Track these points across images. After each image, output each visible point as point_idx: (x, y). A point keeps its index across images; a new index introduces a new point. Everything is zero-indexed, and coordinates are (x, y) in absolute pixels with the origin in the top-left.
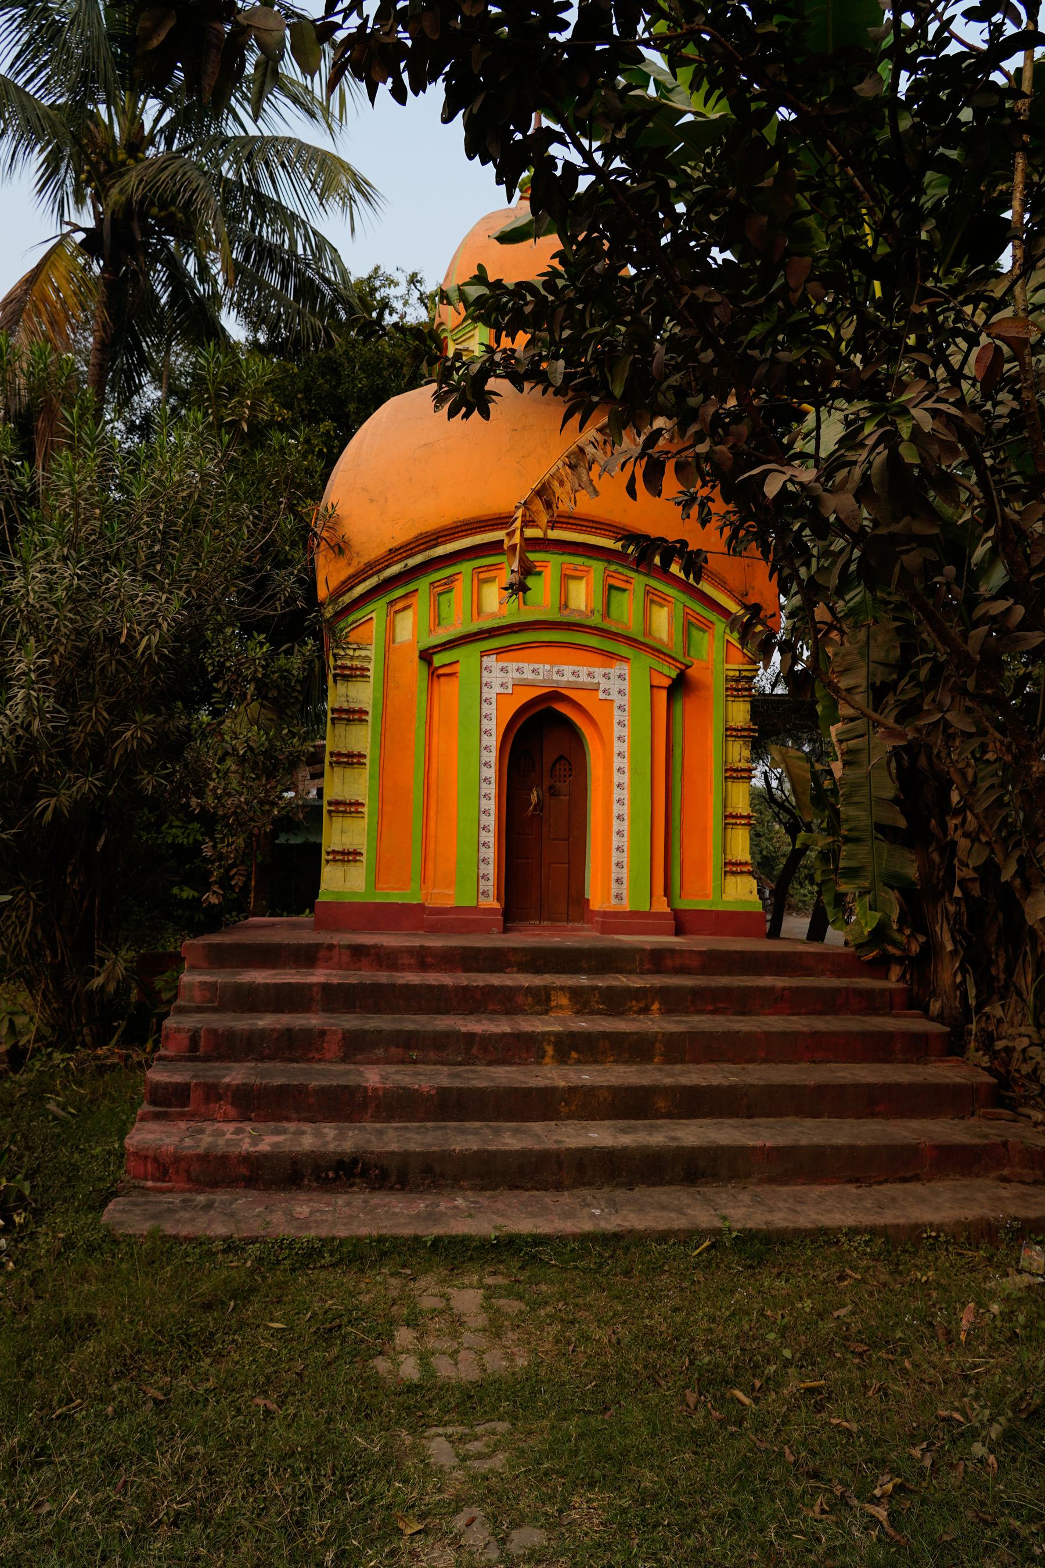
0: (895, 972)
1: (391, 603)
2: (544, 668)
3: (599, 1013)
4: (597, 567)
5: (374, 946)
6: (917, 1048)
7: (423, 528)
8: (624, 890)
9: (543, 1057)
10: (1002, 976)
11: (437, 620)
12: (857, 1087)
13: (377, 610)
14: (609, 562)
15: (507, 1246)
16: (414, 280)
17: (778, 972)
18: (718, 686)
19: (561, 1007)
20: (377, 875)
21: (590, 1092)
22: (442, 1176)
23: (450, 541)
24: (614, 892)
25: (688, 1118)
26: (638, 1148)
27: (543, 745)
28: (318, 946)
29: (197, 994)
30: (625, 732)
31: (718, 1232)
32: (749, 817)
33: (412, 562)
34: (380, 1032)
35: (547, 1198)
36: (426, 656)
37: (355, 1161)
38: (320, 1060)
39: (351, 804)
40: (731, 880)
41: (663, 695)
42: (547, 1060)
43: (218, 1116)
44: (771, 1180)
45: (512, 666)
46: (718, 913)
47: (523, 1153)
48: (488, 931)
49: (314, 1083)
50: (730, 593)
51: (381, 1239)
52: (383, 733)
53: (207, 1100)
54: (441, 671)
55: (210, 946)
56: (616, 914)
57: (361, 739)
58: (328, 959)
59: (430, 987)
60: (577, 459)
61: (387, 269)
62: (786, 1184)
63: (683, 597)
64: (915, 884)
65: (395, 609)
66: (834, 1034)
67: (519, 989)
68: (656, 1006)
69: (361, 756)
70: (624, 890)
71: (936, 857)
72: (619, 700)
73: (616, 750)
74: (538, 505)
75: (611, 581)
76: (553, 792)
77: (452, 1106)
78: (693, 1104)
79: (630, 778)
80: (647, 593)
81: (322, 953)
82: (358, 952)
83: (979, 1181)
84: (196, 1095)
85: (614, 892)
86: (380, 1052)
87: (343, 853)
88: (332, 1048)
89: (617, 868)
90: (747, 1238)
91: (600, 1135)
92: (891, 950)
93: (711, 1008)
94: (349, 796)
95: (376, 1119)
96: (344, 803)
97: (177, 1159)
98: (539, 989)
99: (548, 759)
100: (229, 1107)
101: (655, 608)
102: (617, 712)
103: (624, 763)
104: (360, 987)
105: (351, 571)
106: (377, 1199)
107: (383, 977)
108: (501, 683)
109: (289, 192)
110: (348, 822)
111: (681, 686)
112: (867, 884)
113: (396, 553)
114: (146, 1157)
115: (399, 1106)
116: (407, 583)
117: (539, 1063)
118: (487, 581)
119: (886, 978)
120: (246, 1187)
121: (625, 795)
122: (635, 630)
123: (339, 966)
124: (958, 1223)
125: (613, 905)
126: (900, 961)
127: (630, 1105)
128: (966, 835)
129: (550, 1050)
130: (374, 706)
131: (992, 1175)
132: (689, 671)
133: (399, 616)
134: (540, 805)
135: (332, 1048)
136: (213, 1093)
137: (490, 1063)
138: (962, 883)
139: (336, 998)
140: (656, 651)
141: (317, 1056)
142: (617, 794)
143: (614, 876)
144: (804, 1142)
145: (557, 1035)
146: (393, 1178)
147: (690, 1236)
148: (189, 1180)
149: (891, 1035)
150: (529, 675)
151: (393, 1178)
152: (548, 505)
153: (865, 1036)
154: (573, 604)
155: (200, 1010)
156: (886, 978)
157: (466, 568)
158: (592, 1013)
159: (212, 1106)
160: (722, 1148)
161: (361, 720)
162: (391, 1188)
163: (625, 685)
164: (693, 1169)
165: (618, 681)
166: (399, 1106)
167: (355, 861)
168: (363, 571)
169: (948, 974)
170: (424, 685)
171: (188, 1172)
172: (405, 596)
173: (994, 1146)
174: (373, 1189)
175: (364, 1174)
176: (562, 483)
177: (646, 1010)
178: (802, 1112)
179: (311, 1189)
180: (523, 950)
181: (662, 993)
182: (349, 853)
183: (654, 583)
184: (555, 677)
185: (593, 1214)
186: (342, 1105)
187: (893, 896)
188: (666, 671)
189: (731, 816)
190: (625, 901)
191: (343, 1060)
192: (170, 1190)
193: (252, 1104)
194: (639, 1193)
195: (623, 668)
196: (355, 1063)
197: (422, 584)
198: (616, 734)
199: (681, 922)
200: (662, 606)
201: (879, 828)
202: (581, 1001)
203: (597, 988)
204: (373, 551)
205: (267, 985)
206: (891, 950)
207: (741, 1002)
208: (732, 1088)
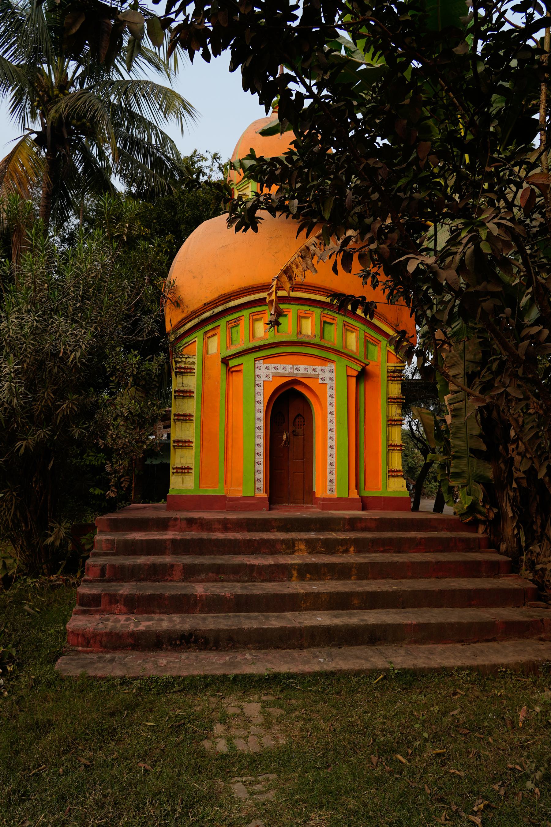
0: (481, 528)
1: (206, 333)
2: (289, 367)
3: (321, 553)
4: (317, 312)
5: (200, 519)
6: (494, 569)
7: (223, 292)
8: (334, 486)
9: (291, 577)
10: (539, 530)
11: (231, 342)
13: (198, 337)
14: (323, 309)
16: (215, 157)
17: (134, 543)
18: (383, 375)
19: (301, 550)
20: (201, 480)
21: (317, 595)
22: (238, 642)
23: (237, 298)
24: (328, 487)
26: (343, 626)
27: (289, 408)
28: (169, 519)
29: (104, 545)
31: (387, 670)
32: (401, 446)
36: (225, 361)
37: (191, 635)
38: (171, 581)
39: (186, 442)
40: (392, 480)
41: (354, 380)
42: (294, 578)
43: (116, 611)
44: (416, 642)
45: (272, 366)
48: (261, 510)
49: (168, 593)
50: (389, 325)
51: (205, 677)
53: (111, 603)
54: (233, 369)
55: (110, 520)
56: (330, 500)
57: (190, 406)
59: (230, 541)
61: (201, 152)
62: (424, 644)
64: (491, 481)
65: (208, 336)
66: (449, 562)
68: (352, 549)
71: (503, 466)
73: (329, 411)
74: (285, 278)
75: (325, 319)
76: (295, 434)
77: (243, 604)
78: (373, 601)
79: (336, 426)
80: (344, 325)
81: (171, 523)
82: (191, 522)
83: (528, 641)
84: (104, 600)
85: (328, 487)
86: (203, 576)
87: (181, 468)
88: (178, 574)
89: (330, 474)
90: (403, 673)
91: (323, 619)
92: (479, 516)
93: (381, 549)
94: (184, 437)
95: (202, 611)
97: (95, 635)
98: (288, 540)
99: (292, 416)
100: (122, 607)
101: (349, 334)
103: (333, 418)
104: (192, 540)
105: (184, 315)
106: (203, 655)
107: (204, 535)
108: (264, 376)
110: (184, 452)
111: (363, 375)
113: (208, 306)
114: (78, 634)
115: (215, 604)
116: (214, 322)
117: (290, 581)
118: (257, 320)
119: (477, 532)
121: (334, 435)
122: (338, 346)
123: (181, 530)
124: (517, 663)
126: (484, 522)
127: (339, 602)
128: (519, 454)
129: (295, 574)
131: (535, 637)
135: (178, 574)
136: (113, 599)
137: (263, 581)
138: (517, 480)
139: (178, 547)
140: (349, 357)
142: (329, 434)
143: (328, 479)
144: (433, 621)
145: (299, 565)
146: (212, 644)
147: (372, 673)
148: (101, 646)
150: (281, 371)
151: (212, 644)
152: (290, 278)
154: (304, 332)
155: (105, 554)
156: (477, 532)
157: (246, 313)
158: (318, 553)
159: (113, 606)
160: (389, 625)
162: (211, 649)
163: (333, 376)
164: (374, 636)
166: (215, 604)
167: (188, 473)
168: (190, 316)
169: (510, 529)
170: (224, 376)
171: (100, 642)
174: (201, 650)
175: (196, 641)
176: (297, 266)
177: (346, 551)
178: (452, 606)
180: (280, 520)
181: (356, 542)
182: (185, 468)
183: (347, 320)
184: (295, 372)
185: (319, 661)
186: (184, 604)
190: (335, 492)
191: (183, 580)
192: (91, 652)
193: (136, 605)
194: (345, 650)
195: (330, 366)
196: (190, 582)
197: (223, 322)
200: (352, 332)
201: (472, 450)
202: (312, 547)
203: (320, 539)
206: (479, 516)
208: (394, 592)
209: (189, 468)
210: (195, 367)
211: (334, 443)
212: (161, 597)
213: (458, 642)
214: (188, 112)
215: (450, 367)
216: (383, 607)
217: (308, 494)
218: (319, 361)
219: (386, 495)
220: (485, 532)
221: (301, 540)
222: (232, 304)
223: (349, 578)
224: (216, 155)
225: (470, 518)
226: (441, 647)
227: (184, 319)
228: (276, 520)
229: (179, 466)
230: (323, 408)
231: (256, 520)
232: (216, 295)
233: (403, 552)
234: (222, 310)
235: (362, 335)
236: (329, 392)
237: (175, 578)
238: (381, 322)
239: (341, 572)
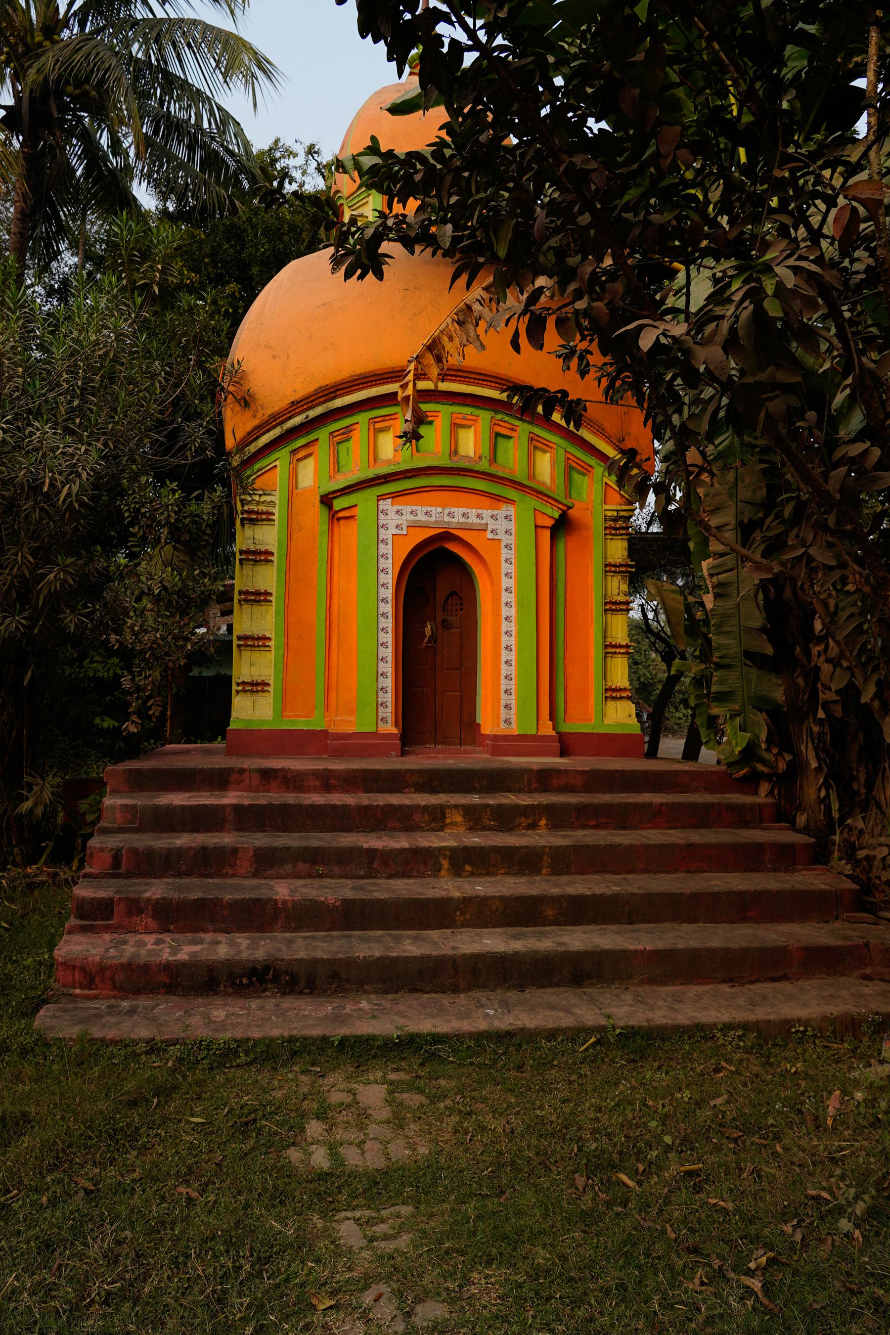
1: (294, 452)
2: (436, 511)
3: (491, 829)
4: (485, 416)
5: (283, 770)
7: (323, 383)
9: (439, 870)
10: (863, 791)
11: (336, 467)
13: (281, 458)
15: (408, 1045)
16: (311, 151)
17: (170, 810)
18: (597, 526)
19: (455, 824)
20: (284, 704)
21: (483, 901)
23: (348, 393)
24: (503, 717)
25: (574, 925)
26: (528, 953)
27: (436, 581)
28: (230, 771)
30: (512, 569)
32: (627, 646)
33: (312, 414)
34: (288, 849)
36: (327, 500)
37: (267, 968)
38: (233, 876)
39: (259, 639)
40: (611, 704)
41: (547, 534)
42: (443, 872)
44: (652, 981)
46: (600, 736)
47: (422, 959)
48: (387, 755)
49: (228, 897)
50: (608, 439)
51: (292, 1040)
53: (130, 913)
54: (340, 515)
56: (506, 738)
58: (239, 782)
59: (334, 807)
60: (465, 317)
61: (287, 141)
62: (665, 984)
65: (297, 457)
67: (416, 808)
68: (543, 822)
71: (801, 681)
72: (505, 539)
74: (429, 359)
76: (446, 625)
78: (578, 912)
79: (517, 612)
80: (531, 440)
81: (233, 777)
82: (267, 776)
83: (843, 980)
84: (119, 909)
85: (503, 717)
86: (288, 867)
87: (252, 684)
88: (245, 864)
89: (506, 694)
90: (630, 1034)
91: (493, 942)
92: (761, 768)
93: (594, 823)
94: (257, 631)
95: (285, 929)
96: (252, 638)
98: (434, 807)
100: (150, 920)
101: (539, 454)
104: (270, 807)
105: (256, 422)
106: (288, 1003)
107: (291, 798)
108: (395, 526)
109: (195, 71)
111: (563, 526)
113: (298, 406)
114: (74, 967)
116: (308, 433)
118: (382, 430)
119: (756, 793)
120: (167, 993)
122: (520, 475)
123: (250, 789)
124: (824, 1018)
125: (502, 729)
126: (768, 777)
127: (521, 913)
128: (828, 661)
129: (445, 864)
130: (279, 548)
133: (301, 464)
134: (434, 637)
135: (245, 864)
136: (135, 907)
137: (390, 877)
138: (826, 706)
139: (248, 818)
140: (540, 494)
142: (505, 626)
144: (681, 945)
145: (453, 850)
146: (302, 984)
147: (577, 1033)
148: (114, 987)
149: (761, 845)
150: (422, 517)
151: (302, 984)
152: (439, 359)
153: (736, 847)
154: (462, 451)
155: (121, 830)
156: (756, 793)
157: (363, 418)
158: (484, 828)
159: (134, 918)
160: (605, 952)
161: (267, 561)
162: (301, 993)
163: (512, 526)
164: (579, 971)
167: (263, 691)
168: (267, 422)
169: (812, 789)
170: (325, 527)
171: (112, 979)
172: (306, 445)
174: (284, 994)
175: (276, 979)
176: (451, 339)
177: (534, 826)
179: (226, 994)
180: (420, 772)
181: (548, 810)
182: (257, 684)
183: (537, 430)
184: (447, 519)
186: (255, 916)
188: (549, 511)
190: (514, 726)
191: (255, 875)
192: (96, 997)
193: (172, 917)
195: (506, 510)
196: (265, 878)
197: (323, 434)
198: (503, 571)
200: (545, 452)
202: (474, 818)
203: (488, 805)
206: (761, 768)
207: (620, 817)
209: (265, 684)
210: (276, 511)
211: (512, 641)
212: (216, 903)
213: (724, 981)
214: (265, 72)
216: (594, 921)
217: (467, 728)
218: (487, 501)
219: (601, 731)
220: (770, 793)
221: (456, 807)
222: (339, 403)
223: (538, 872)
224: (312, 146)
225: (746, 769)
228: (412, 772)
229: (248, 680)
230: (495, 582)
231: (378, 772)
233: (630, 828)
234: (321, 412)
235: (561, 458)
236: (504, 553)
237: (241, 871)
238: (594, 434)
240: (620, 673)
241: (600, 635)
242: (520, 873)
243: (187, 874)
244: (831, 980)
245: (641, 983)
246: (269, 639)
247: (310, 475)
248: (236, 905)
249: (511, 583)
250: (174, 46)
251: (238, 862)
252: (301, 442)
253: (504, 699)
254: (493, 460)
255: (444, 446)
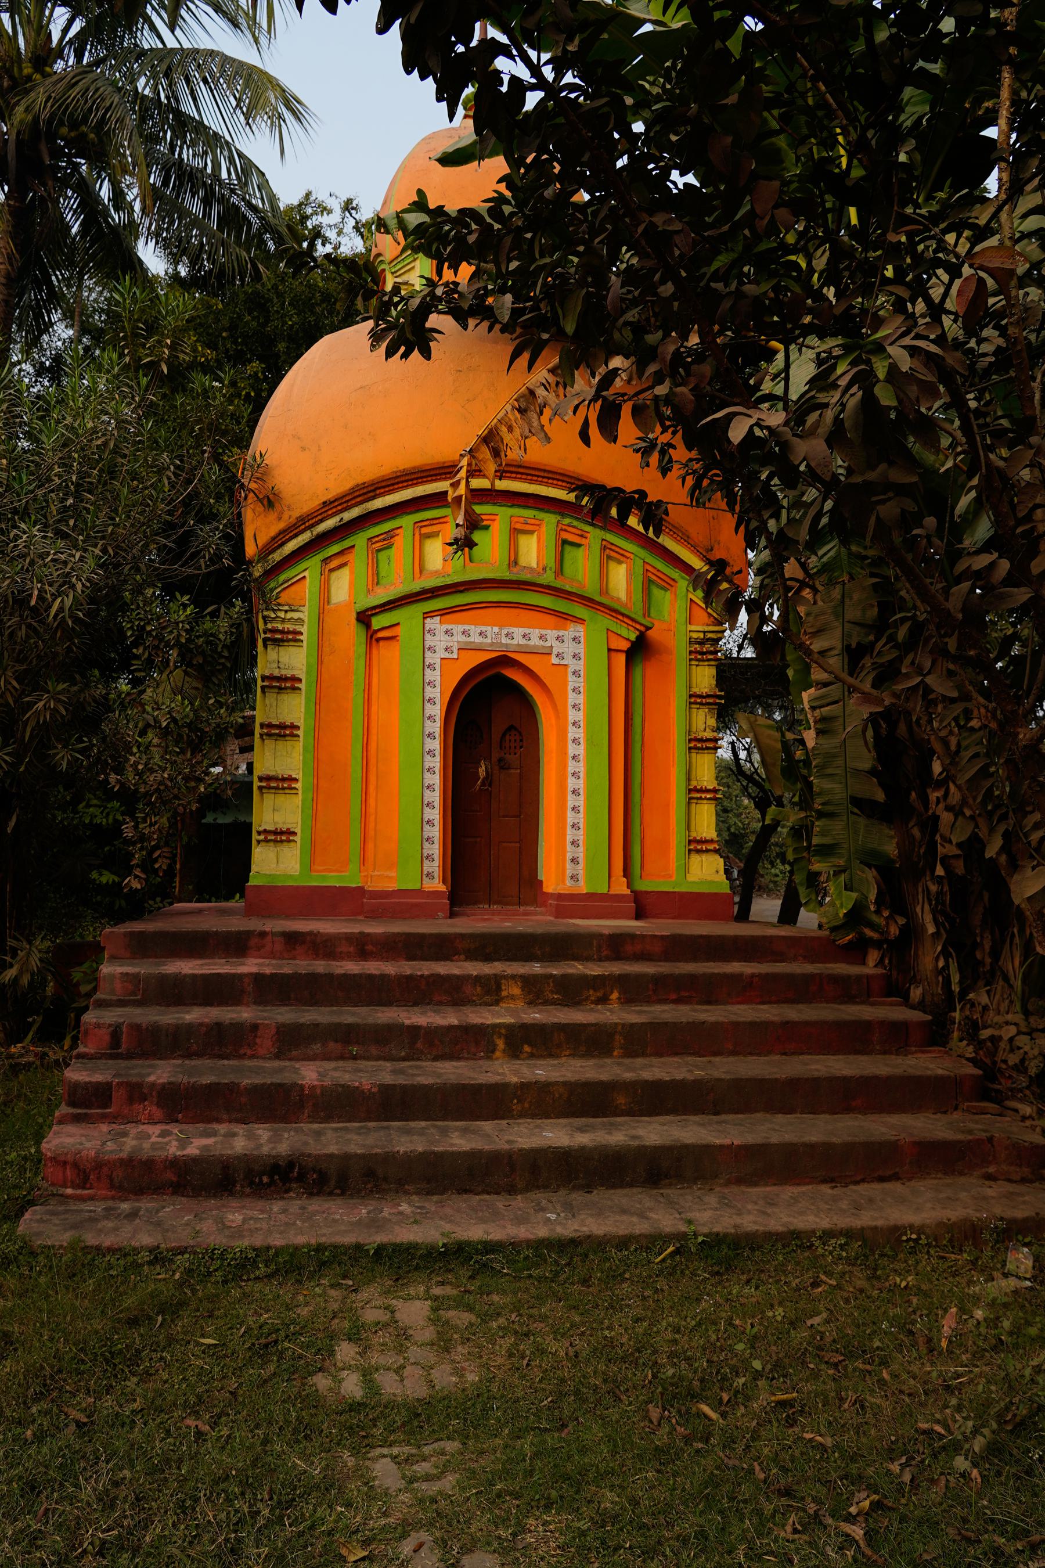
0: (873, 957)
1: (326, 561)
2: (492, 631)
3: (554, 1003)
7: (360, 480)
8: (580, 870)
9: (493, 1051)
10: (988, 960)
11: (376, 579)
12: (832, 1080)
13: (310, 569)
15: (456, 1255)
16: (349, 206)
18: (681, 649)
19: (512, 997)
20: (313, 857)
21: (544, 1088)
22: (385, 1179)
23: (390, 492)
24: (569, 873)
26: (596, 1148)
27: (492, 712)
32: (715, 791)
33: (348, 516)
35: (499, 1202)
36: (364, 618)
37: (291, 1164)
38: (252, 1057)
39: (283, 780)
40: (695, 859)
41: (622, 658)
42: (498, 1054)
44: (739, 1181)
45: (458, 629)
46: (682, 895)
47: (472, 1154)
48: (433, 916)
49: (246, 1082)
50: (694, 548)
51: (320, 1248)
52: (318, 702)
53: (131, 1100)
56: (572, 897)
57: (293, 709)
59: (370, 977)
60: (527, 403)
61: (320, 195)
63: (642, 553)
64: (894, 862)
65: (329, 567)
66: (807, 1023)
68: (615, 996)
69: (294, 727)
70: (580, 870)
71: (916, 832)
72: (573, 665)
74: (485, 453)
76: (503, 765)
78: (656, 1099)
80: (604, 548)
81: (253, 942)
82: (292, 939)
83: (963, 1180)
84: (118, 1096)
85: (569, 873)
86: (317, 1047)
87: (275, 833)
88: (266, 1043)
89: (572, 846)
90: (715, 1242)
91: (556, 1135)
92: (869, 933)
93: (674, 996)
95: (313, 1118)
97: (99, 1165)
98: (488, 977)
100: (154, 1108)
101: (612, 565)
102: (571, 678)
104: (296, 977)
105: (282, 525)
106: (315, 1205)
108: (442, 649)
110: (281, 799)
111: (640, 649)
112: (842, 862)
114: (65, 1163)
116: (343, 539)
117: (489, 1058)
118: (429, 536)
119: (863, 962)
122: (591, 589)
123: (272, 955)
124: (940, 1224)
125: (568, 886)
126: (878, 944)
127: (588, 1102)
128: (948, 809)
129: (501, 1044)
130: (308, 673)
132: (649, 632)
133: (334, 575)
134: (489, 779)
135: (266, 1043)
136: (137, 1093)
137: (436, 1059)
138: (945, 861)
139: (270, 989)
140: (613, 612)
141: (249, 1052)
143: (569, 856)
145: (509, 1027)
146: (333, 1183)
147: (653, 1242)
148: (112, 1187)
151: (333, 1183)
152: (496, 453)
153: (840, 1025)
154: (523, 561)
155: (121, 1003)
156: (863, 962)
157: (407, 521)
158: (546, 1003)
159: (136, 1106)
160: (686, 1147)
161: (294, 689)
162: (331, 1194)
163: (580, 649)
164: (656, 1170)
165: (572, 645)
167: (289, 841)
168: (294, 526)
169: (929, 958)
170: (362, 649)
171: (110, 1178)
173: (979, 1141)
174: (311, 1195)
175: (301, 1178)
176: (510, 429)
177: (604, 1000)
179: (243, 1195)
181: (622, 981)
182: (282, 833)
183: (610, 537)
184: (504, 640)
186: (277, 1104)
187: (870, 874)
188: (624, 633)
189: (696, 790)
190: (581, 883)
191: (277, 1056)
192: (92, 1198)
193: (180, 1104)
195: (574, 630)
196: (290, 1059)
197: (360, 540)
198: (571, 702)
199: (642, 905)
200: (620, 562)
201: (856, 801)
202: (534, 990)
203: (551, 976)
204: (305, 504)
205: (194, 976)
206: (869, 933)
207: (707, 991)
210: (304, 629)
212: (232, 1088)
213: (824, 1181)
215: (815, 634)
216: (673, 1111)
218: (551, 619)
219: (684, 889)
220: (880, 963)
221: (513, 977)
222: (379, 503)
224: (349, 201)
225: (852, 935)
226: (789, 1191)
227: (281, 532)
228: (462, 936)
229: (270, 827)
230: (560, 715)
231: (422, 937)
232: (347, 486)
233: (716, 1002)
234: (359, 514)
235: (639, 569)
236: (572, 681)
239: (593, 1042)
240: (706, 822)
241: (683, 778)
242: (588, 1055)
243: (199, 1055)
244: (948, 1180)
245: (728, 1183)
246: (296, 780)
247: (346, 588)
248: (256, 1090)
249: (579, 716)
250: (188, 80)
251: (258, 1040)
252: (335, 549)
253: (570, 851)
254: (559, 571)
255: (502, 555)
